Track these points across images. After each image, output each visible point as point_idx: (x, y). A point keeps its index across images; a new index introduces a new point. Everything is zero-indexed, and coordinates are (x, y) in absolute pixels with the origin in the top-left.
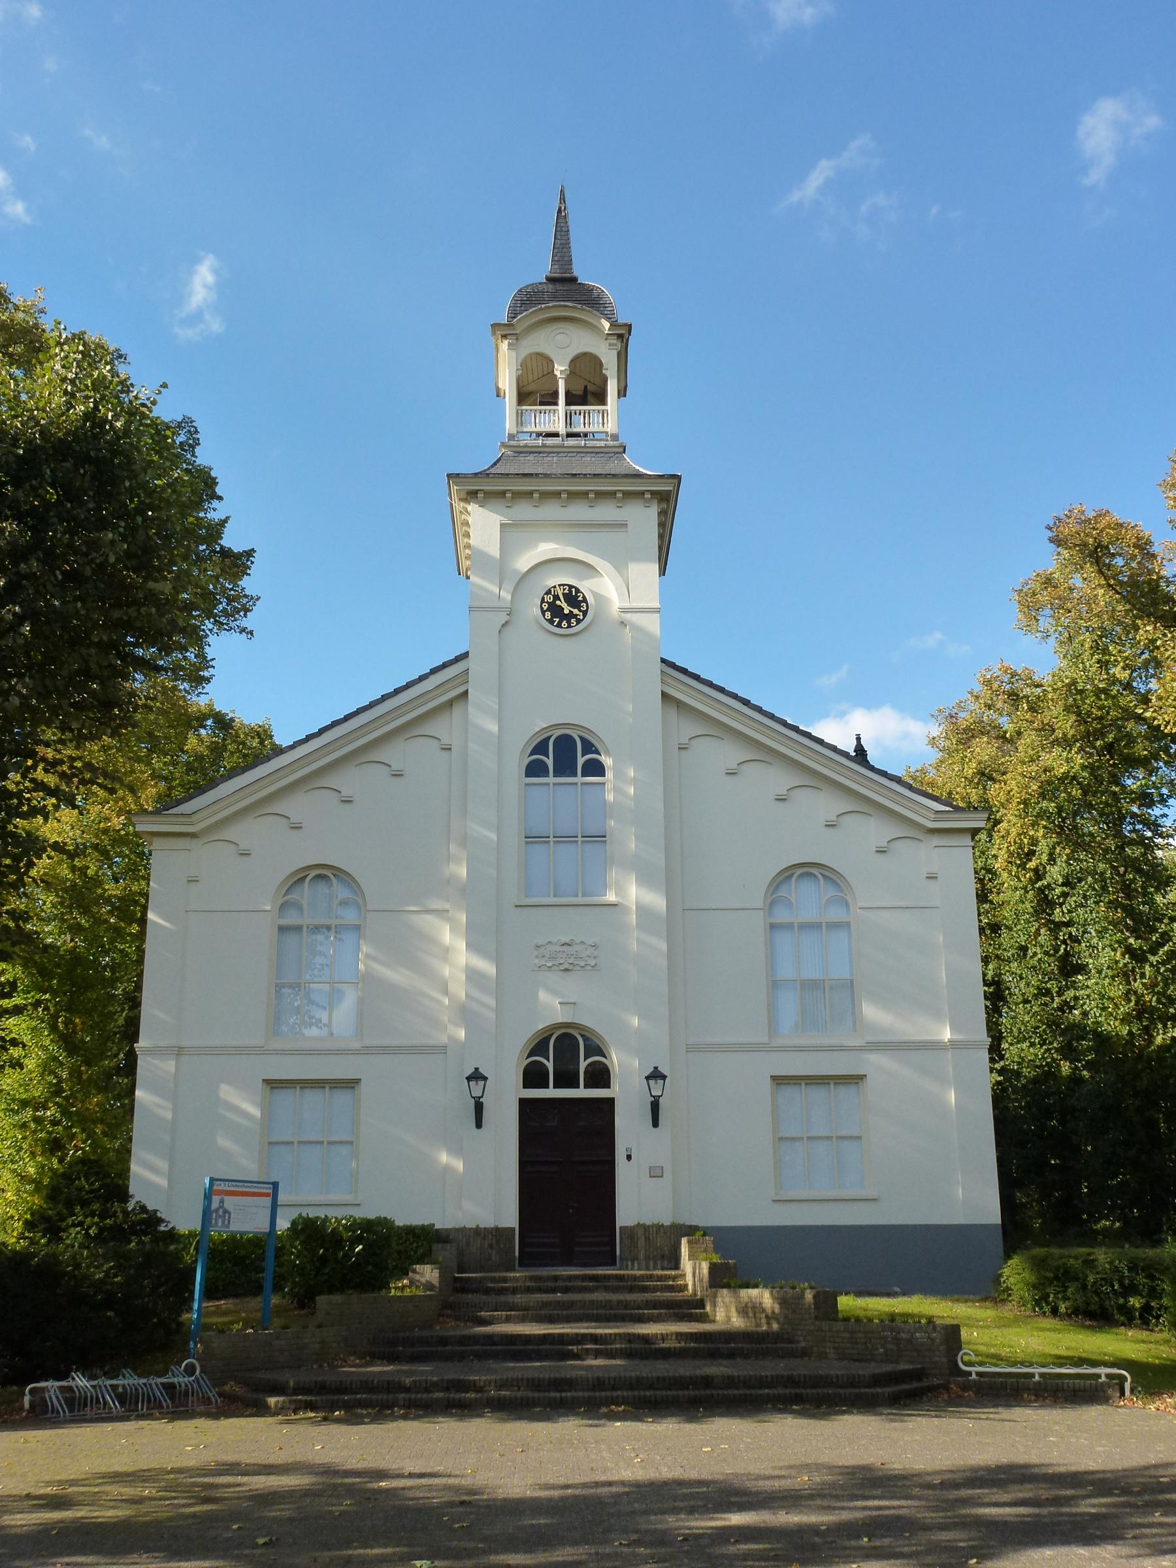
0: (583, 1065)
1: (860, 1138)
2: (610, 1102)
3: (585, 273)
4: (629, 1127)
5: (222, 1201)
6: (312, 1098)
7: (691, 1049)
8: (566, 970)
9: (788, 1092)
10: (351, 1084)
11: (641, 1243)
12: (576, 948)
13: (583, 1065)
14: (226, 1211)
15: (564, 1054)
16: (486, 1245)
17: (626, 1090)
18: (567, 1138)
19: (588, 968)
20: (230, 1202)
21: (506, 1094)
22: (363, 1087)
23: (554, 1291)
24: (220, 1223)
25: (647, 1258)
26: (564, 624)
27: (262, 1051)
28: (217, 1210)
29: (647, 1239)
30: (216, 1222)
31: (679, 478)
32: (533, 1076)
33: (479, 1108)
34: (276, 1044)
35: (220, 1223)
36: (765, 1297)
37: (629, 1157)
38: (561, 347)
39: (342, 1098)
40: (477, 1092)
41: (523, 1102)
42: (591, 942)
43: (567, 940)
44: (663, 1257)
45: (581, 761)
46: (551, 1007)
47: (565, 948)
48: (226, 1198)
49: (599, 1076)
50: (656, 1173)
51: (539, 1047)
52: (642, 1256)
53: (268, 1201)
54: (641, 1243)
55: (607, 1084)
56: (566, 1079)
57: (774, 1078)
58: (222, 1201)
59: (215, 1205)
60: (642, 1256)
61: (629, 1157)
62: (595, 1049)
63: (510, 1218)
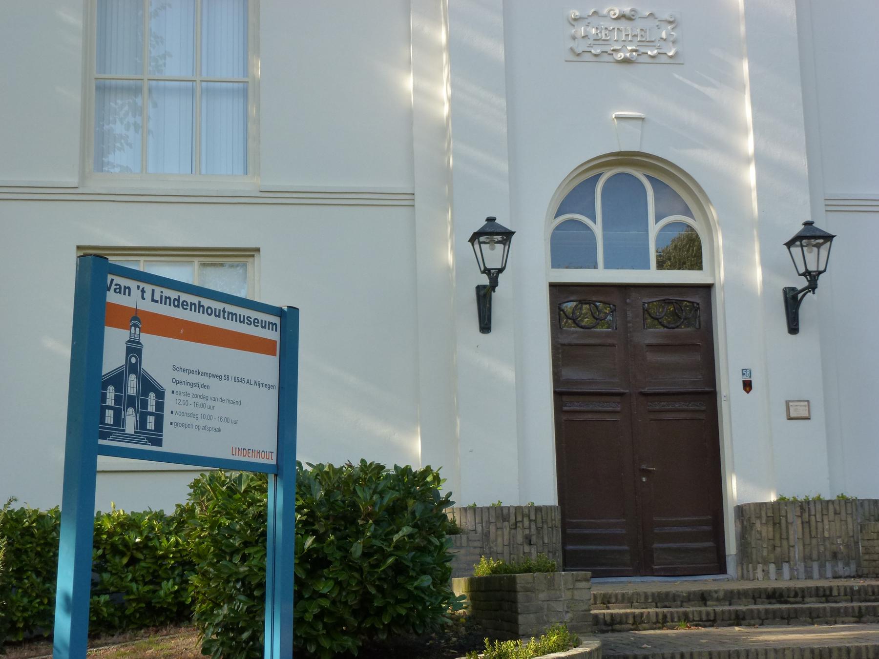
2: (707, 289)
4: (744, 337)
5: (134, 349)
8: (626, 61)
11: (796, 531)
12: (639, 24)
14: (148, 385)
16: (520, 538)
17: (742, 273)
19: (663, 59)
20: (161, 357)
24: (130, 427)
25: (807, 558)
28: (117, 380)
29: (806, 524)
30: (119, 420)
34: (96, 185)
35: (130, 427)
37: (747, 386)
41: (558, 290)
42: (666, 17)
43: (627, 10)
44: (835, 555)
46: (620, 117)
47: (623, 24)
48: (148, 341)
52: (797, 553)
53: (267, 367)
54: (796, 531)
55: (697, 265)
58: (134, 349)
59: (113, 358)
60: (797, 553)
61: (747, 386)
63: (546, 494)
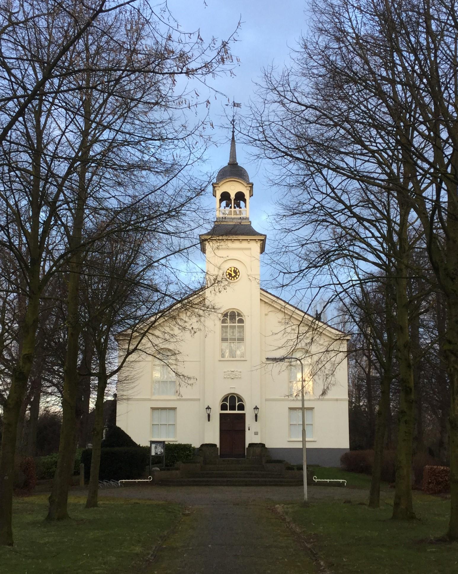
0: (237, 404)
1: (312, 424)
3: (241, 161)
4: (249, 421)
6: (164, 412)
7: (266, 400)
9: (156, 412)
10: (174, 409)
13: (237, 404)
15: (232, 401)
17: (249, 412)
18: (233, 418)
21: (216, 412)
22: (178, 409)
23: (228, 481)
26: (233, 279)
27: (149, 400)
31: (266, 236)
32: (223, 407)
33: (209, 416)
36: (44, 208)
37: (249, 429)
38: (233, 188)
39: (172, 412)
40: (256, 413)
43: (232, 370)
45: (237, 319)
49: (241, 407)
50: (256, 434)
51: (225, 399)
55: (244, 410)
56: (233, 408)
57: (289, 408)
61: (249, 429)
62: (240, 399)
